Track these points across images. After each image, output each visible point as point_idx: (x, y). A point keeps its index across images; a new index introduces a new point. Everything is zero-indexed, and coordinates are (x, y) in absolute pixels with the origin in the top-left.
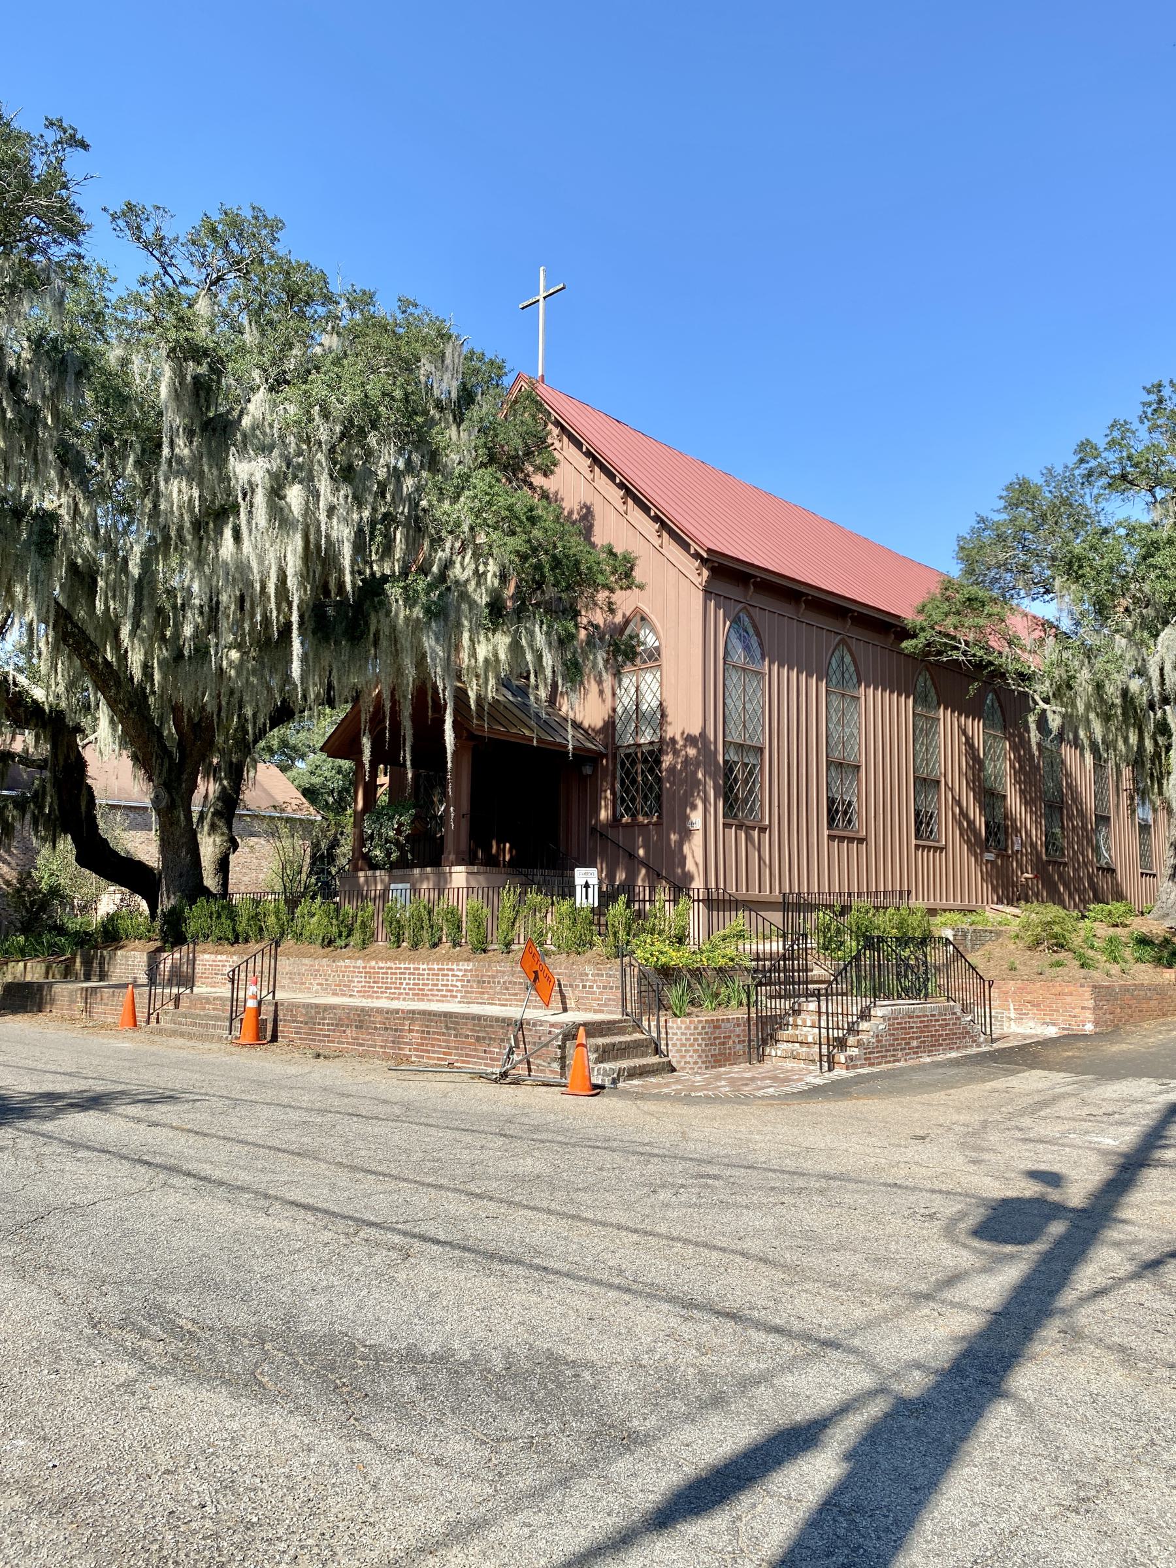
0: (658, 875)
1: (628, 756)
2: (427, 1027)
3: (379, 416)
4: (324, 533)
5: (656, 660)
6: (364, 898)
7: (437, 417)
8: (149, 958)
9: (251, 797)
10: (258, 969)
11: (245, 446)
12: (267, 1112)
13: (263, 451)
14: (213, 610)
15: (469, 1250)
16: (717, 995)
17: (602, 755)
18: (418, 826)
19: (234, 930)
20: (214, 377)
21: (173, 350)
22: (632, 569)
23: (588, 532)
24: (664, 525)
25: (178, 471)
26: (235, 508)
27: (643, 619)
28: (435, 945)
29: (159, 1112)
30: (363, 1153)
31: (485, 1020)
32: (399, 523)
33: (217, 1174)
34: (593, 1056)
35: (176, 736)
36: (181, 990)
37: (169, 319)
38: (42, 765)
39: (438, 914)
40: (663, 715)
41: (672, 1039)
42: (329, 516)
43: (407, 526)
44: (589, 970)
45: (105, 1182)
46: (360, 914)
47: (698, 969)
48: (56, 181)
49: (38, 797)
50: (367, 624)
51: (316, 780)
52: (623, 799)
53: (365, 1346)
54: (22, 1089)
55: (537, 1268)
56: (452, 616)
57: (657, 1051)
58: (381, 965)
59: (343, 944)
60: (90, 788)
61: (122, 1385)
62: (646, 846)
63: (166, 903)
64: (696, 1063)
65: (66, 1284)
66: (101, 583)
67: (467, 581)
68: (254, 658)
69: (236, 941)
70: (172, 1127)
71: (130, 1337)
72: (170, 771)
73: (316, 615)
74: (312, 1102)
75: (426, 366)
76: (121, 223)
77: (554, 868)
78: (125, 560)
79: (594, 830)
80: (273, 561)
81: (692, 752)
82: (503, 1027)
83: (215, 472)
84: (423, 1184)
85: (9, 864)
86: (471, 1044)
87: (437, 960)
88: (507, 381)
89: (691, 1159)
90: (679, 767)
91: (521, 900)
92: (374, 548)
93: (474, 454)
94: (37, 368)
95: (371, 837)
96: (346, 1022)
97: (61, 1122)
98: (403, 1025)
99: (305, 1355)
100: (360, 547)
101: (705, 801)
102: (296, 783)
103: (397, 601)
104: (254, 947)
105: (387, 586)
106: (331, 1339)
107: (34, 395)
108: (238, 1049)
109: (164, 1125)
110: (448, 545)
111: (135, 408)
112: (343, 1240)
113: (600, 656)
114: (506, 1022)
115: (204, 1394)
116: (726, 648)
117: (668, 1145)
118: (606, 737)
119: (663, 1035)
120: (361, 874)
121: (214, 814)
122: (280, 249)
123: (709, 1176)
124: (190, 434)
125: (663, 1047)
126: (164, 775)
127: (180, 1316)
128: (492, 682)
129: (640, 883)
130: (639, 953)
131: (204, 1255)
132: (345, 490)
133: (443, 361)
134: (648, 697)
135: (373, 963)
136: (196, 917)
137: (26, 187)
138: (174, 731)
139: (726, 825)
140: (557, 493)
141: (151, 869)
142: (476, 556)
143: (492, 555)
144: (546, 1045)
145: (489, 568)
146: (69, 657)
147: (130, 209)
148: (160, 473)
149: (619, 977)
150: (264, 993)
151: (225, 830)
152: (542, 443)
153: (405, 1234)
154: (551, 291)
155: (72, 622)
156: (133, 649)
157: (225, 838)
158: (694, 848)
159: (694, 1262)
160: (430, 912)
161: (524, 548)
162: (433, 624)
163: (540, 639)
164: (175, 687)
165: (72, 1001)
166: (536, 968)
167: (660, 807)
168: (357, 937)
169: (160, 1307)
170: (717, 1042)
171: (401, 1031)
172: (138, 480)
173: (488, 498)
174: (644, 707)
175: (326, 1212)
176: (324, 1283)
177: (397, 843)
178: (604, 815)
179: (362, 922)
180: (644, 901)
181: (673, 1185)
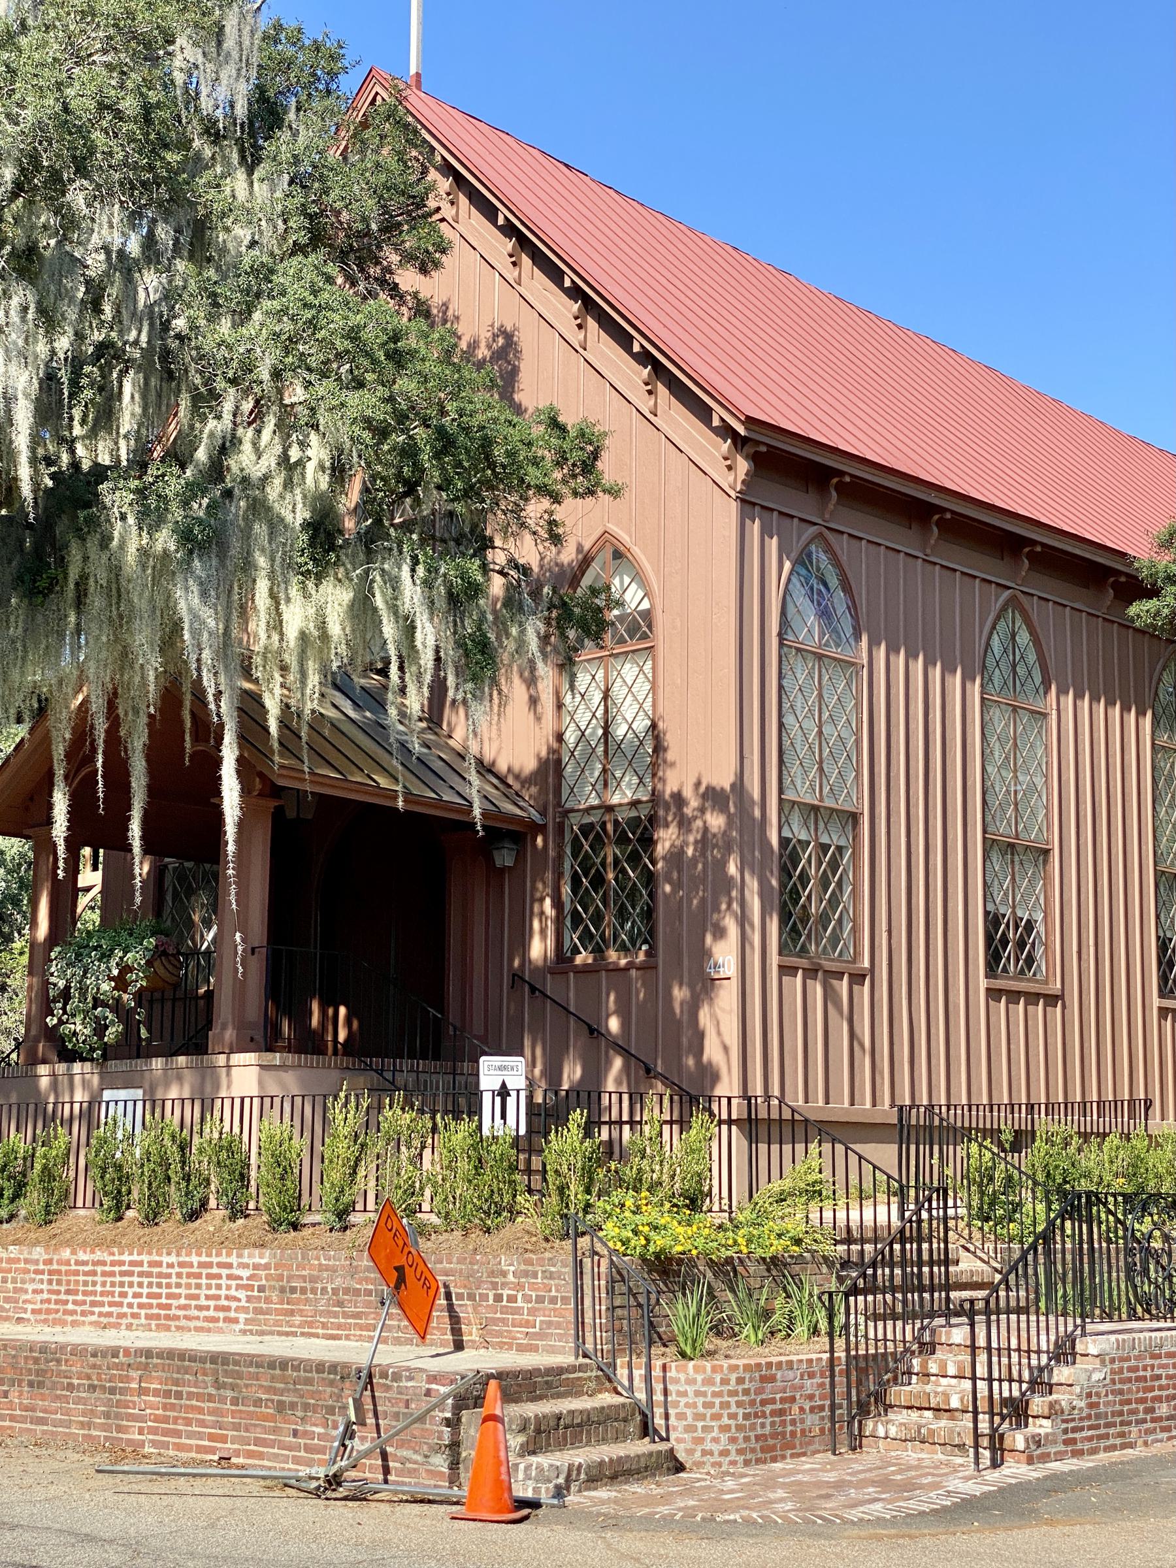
1: (586, 829)
2: (176, 1383)
5: (645, 637)
6: (49, 1120)
16: (767, 1314)
18: (161, 971)
22: (595, 455)
23: (506, 384)
27: (618, 555)
28: (193, 1215)
31: (296, 1368)
32: (128, 364)
40: (659, 748)
41: (676, 1404)
43: (145, 368)
44: (510, 1265)
46: (40, 1151)
47: (729, 1261)
50: (62, 563)
57: (646, 1429)
58: (82, 1256)
62: (624, 1012)
64: (724, 1453)
67: (266, 478)
77: (436, 1057)
79: (517, 978)
81: (716, 821)
82: (332, 1383)
86: (266, 1418)
87: (198, 1247)
88: (348, 84)
90: (690, 852)
92: (77, 413)
93: (281, 226)
95: (66, 995)
101: (743, 921)
103: (123, 517)
105: (103, 487)
110: (228, 407)
113: (533, 628)
114: (337, 1372)
116: (783, 613)
118: (543, 791)
119: (658, 1397)
120: (43, 1070)
125: (659, 1421)
128: (314, 679)
129: (610, 1086)
133: (219, 44)
134: (629, 710)
135: (66, 1253)
140: (445, 305)
142: (285, 428)
143: (315, 427)
144: (421, 1419)
145: (309, 453)
149: (569, 1278)
160: (184, 1147)
161: (381, 414)
163: (412, 594)
167: (652, 932)
168: (34, 1198)
170: (768, 1409)
171: (123, 1391)
173: (308, 314)
174: (620, 731)
177: (117, 1007)
178: (539, 948)
179: (45, 1168)
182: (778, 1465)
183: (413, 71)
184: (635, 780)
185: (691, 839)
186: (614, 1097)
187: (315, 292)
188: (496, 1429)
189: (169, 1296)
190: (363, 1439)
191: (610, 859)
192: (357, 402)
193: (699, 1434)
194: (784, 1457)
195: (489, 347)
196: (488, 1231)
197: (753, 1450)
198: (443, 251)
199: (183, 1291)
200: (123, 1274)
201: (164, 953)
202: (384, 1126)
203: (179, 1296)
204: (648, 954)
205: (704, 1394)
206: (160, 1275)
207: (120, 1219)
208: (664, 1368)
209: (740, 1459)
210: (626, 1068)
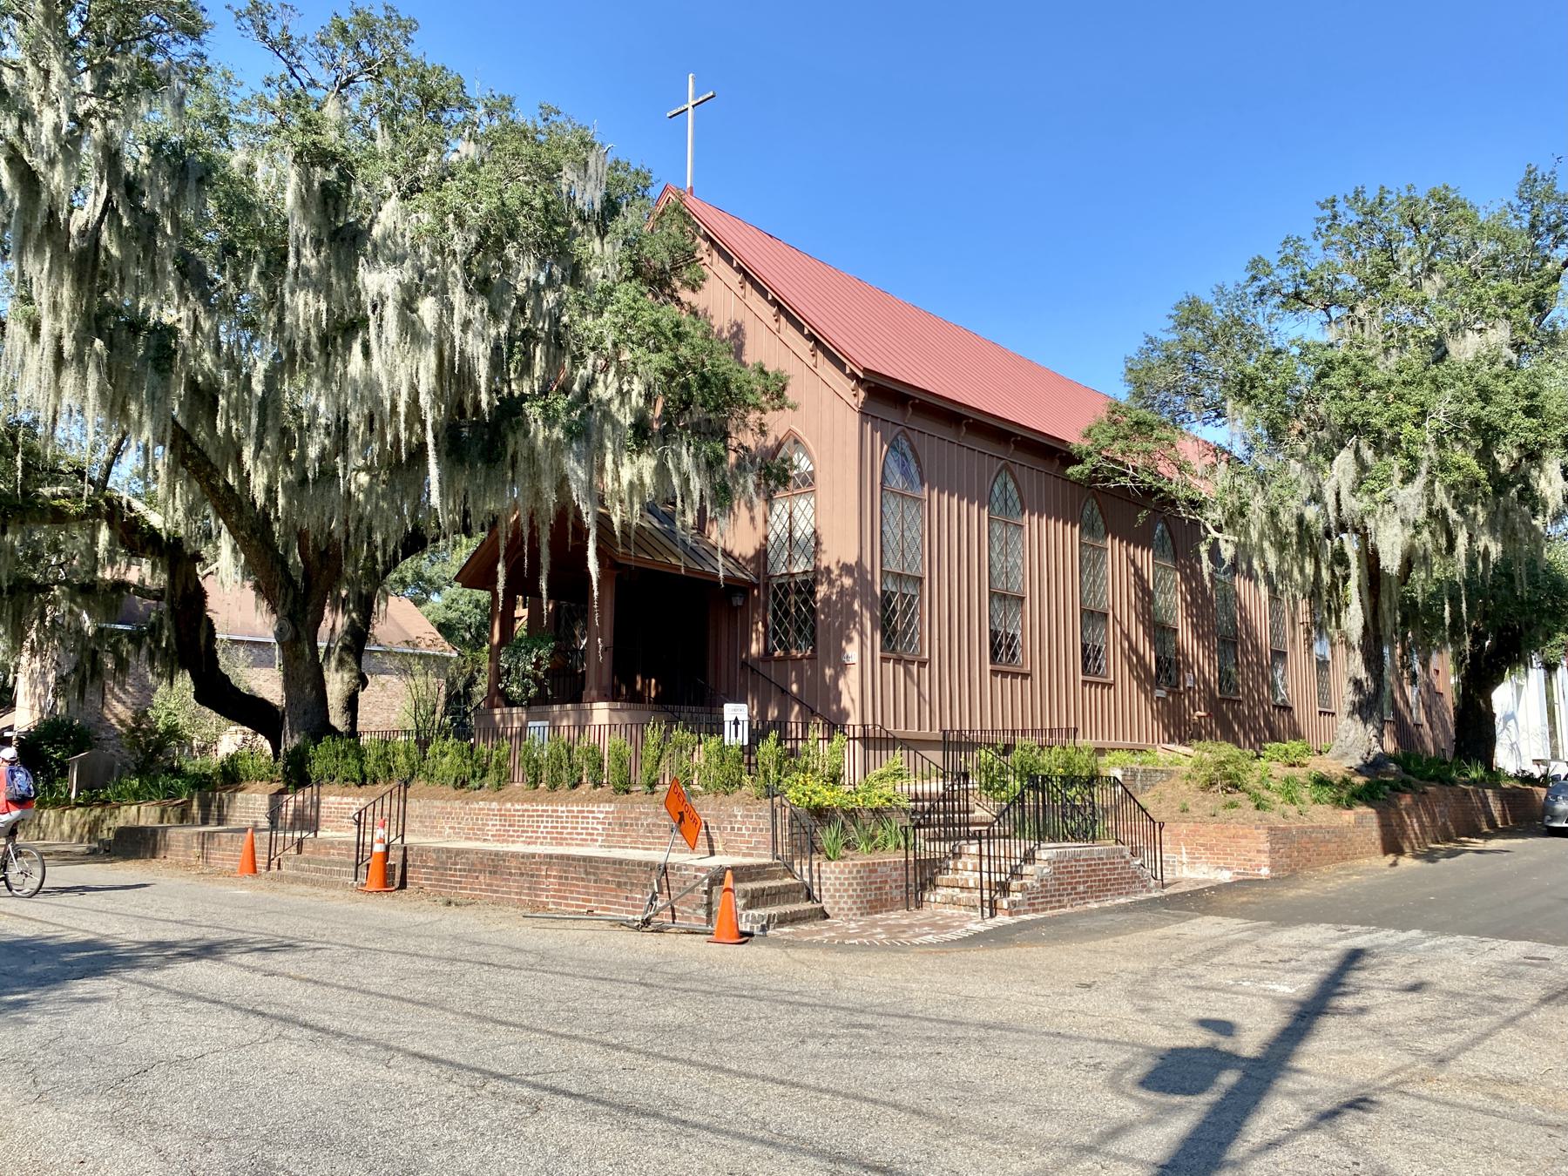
0: (812, 712)
1: (780, 586)
2: (565, 872)
3: (517, 225)
4: (457, 349)
5: (810, 485)
7: (580, 229)
8: (271, 800)
10: (386, 812)
12: (392, 961)
13: (394, 262)
14: (341, 431)
16: (873, 838)
17: (753, 586)
19: (361, 771)
20: (344, 184)
21: (299, 155)
22: (784, 388)
23: (738, 351)
25: (304, 283)
28: (575, 786)
29: (277, 960)
30: (493, 1003)
31: (627, 864)
33: (336, 1025)
34: (741, 902)
37: (296, 122)
38: (158, 595)
39: (578, 752)
40: (818, 543)
42: (464, 331)
43: (547, 343)
44: (739, 812)
45: (215, 1033)
47: (853, 810)
49: (155, 631)
51: (452, 615)
54: (130, 937)
55: (676, 1121)
56: (595, 437)
57: (809, 897)
59: (477, 785)
60: (210, 621)
62: (799, 682)
63: (290, 742)
65: (168, 1140)
66: (222, 402)
67: (610, 400)
68: (384, 482)
69: (364, 782)
72: (295, 601)
75: (568, 175)
77: (702, 705)
78: (248, 377)
79: (744, 664)
80: (403, 378)
81: (848, 582)
82: (645, 872)
83: (344, 284)
84: (556, 1035)
86: (611, 890)
87: (577, 802)
88: (654, 192)
89: (843, 1008)
93: (618, 267)
94: (156, 173)
95: (508, 672)
96: (479, 867)
97: (171, 971)
101: (862, 634)
102: (431, 617)
103: (536, 421)
104: (382, 788)
105: (526, 405)
109: (282, 974)
110: (590, 362)
112: (469, 1093)
113: (751, 479)
114: (649, 866)
116: (883, 472)
118: (758, 565)
119: (816, 880)
120: (497, 711)
121: (342, 649)
122: (414, 51)
124: (318, 243)
125: (816, 893)
126: (289, 606)
128: (637, 507)
129: (793, 719)
132: (481, 303)
135: (509, 805)
136: (322, 758)
138: (299, 559)
139: (883, 659)
140: (706, 310)
142: (620, 373)
143: (636, 373)
148: (286, 285)
149: (770, 819)
150: (393, 837)
152: (690, 257)
153: (535, 1086)
154: (701, 99)
155: (191, 444)
156: (256, 471)
157: (354, 674)
160: (569, 751)
161: (670, 366)
162: (574, 445)
163: (687, 462)
165: (188, 847)
168: (492, 778)
170: (873, 887)
171: (538, 876)
173: (632, 312)
174: (797, 534)
175: (451, 1064)
176: (447, 1138)
177: (536, 679)
178: (755, 648)
182: (878, 916)
186: (794, 725)
187: (635, 301)
189: (562, 828)
196: (727, 794)
201: (559, 651)
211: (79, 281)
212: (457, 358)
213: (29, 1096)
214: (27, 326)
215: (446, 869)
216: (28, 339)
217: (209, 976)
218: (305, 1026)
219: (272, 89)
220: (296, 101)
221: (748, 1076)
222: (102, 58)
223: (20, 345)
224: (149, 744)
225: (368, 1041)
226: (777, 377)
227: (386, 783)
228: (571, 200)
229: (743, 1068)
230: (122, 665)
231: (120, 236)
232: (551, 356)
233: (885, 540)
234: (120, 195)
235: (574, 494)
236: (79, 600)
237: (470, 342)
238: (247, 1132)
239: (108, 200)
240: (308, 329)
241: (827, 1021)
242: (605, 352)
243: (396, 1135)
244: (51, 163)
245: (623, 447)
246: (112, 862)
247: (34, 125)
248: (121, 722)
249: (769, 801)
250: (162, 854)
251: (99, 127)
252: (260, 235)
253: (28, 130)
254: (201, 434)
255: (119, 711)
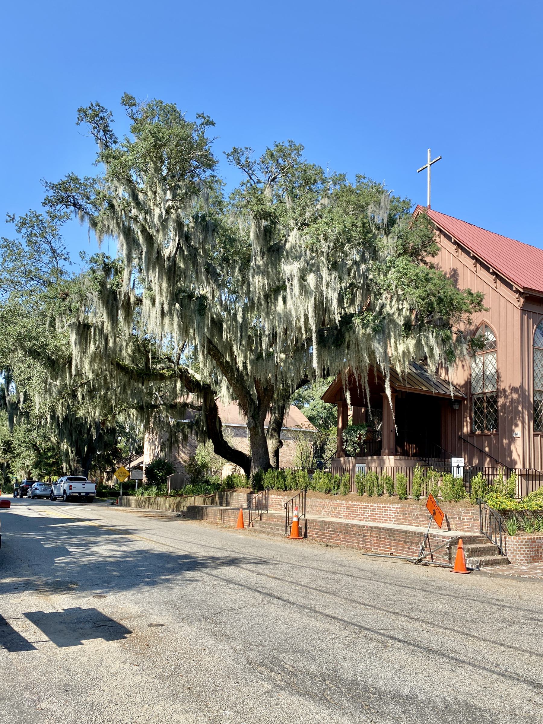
0: (496, 461)
1: (478, 399)
2: (379, 535)
3: (351, 236)
4: (325, 296)
5: (494, 348)
6: (344, 471)
7: (377, 233)
8: (248, 496)
9: (288, 422)
10: (297, 503)
11: (288, 258)
12: (308, 572)
13: (296, 259)
14: (274, 336)
15: (416, 646)
16: (532, 525)
17: (464, 399)
18: (369, 436)
19: (285, 484)
20: (273, 226)
21: (255, 215)
22: (481, 301)
23: (455, 282)
24: (497, 276)
25: (258, 272)
26: (284, 288)
27: (486, 326)
28: (380, 495)
29: (261, 568)
30: (357, 594)
31: (409, 533)
32: (358, 288)
33: (291, 599)
34: (466, 554)
35: (256, 394)
36: (263, 512)
37: (254, 201)
38: (199, 409)
39: (382, 480)
41: (508, 547)
42: (327, 288)
43: (362, 288)
44: (462, 510)
45: (243, 599)
46: (343, 478)
47: (522, 511)
48: (202, 143)
49: (197, 422)
50: (343, 338)
51: (315, 413)
52: (476, 422)
53: (373, 688)
54: (201, 554)
55: (453, 659)
56: (387, 332)
57: (500, 553)
58: (354, 503)
59: (335, 493)
60: (219, 419)
61: (266, 692)
62: (489, 446)
63: (254, 471)
64: (522, 560)
65: (234, 643)
66: (225, 326)
67: (394, 314)
68: (291, 357)
69: (286, 490)
70: (268, 576)
71: (266, 671)
72: (254, 410)
73: (319, 335)
74: (329, 568)
75: (371, 208)
76: (231, 158)
77: (439, 458)
78: (235, 315)
79: (460, 438)
80: (302, 311)
81: (515, 396)
82: (418, 537)
83: (274, 271)
84: (388, 612)
85: (184, 453)
86: (402, 544)
87: (382, 502)
88: (411, 210)
89: (527, 610)
90: (508, 404)
91: (425, 474)
92: (345, 301)
93: (395, 249)
94: (196, 230)
95: (346, 441)
96: (339, 530)
97: (220, 570)
98: (367, 533)
99: (345, 688)
100: (340, 301)
101: (523, 422)
102: (305, 414)
103: (358, 326)
104: (294, 492)
105: (353, 319)
106: (356, 683)
107: (195, 243)
108: (290, 540)
109: (264, 575)
110: (384, 296)
111: (238, 244)
112: (354, 636)
113: (465, 347)
114: (419, 535)
115: (303, 701)
116: (534, 340)
117: (512, 601)
118: (466, 389)
119: (503, 545)
120: (342, 459)
122: (301, 160)
123: (538, 620)
124: (263, 254)
125: (504, 551)
126: (252, 412)
127: (286, 664)
128: (407, 363)
129: (486, 466)
130: (489, 502)
131: (292, 637)
132: (335, 274)
133: (380, 204)
134: (490, 368)
135: (350, 502)
136: (268, 478)
137: (191, 148)
138: (256, 392)
139: (535, 435)
140: (438, 264)
141: (246, 455)
142: (398, 300)
143: (406, 299)
144: (441, 547)
145: (404, 306)
146: (211, 361)
147: (235, 151)
148: (250, 274)
149: (479, 514)
150: (300, 514)
151: (277, 437)
152: (431, 240)
153: (383, 635)
154: (434, 161)
155: (212, 345)
156: (239, 355)
157: (277, 441)
158: (517, 447)
159: (537, 664)
160: (377, 479)
161: (424, 295)
162: (377, 336)
163: (432, 341)
164: (257, 372)
165: (216, 515)
166: (434, 508)
167: (497, 426)
168: (342, 489)
169: (277, 659)
170: (534, 549)
171: (366, 536)
172: (240, 278)
173: (405, 271)
174: (488, 373)
175: (344, 621)
176: (349, 655)
177: (359, 444)
178: (465, 430)
179: (344, 482)
180: (488, 475)
181: (519, 623)
182: (537, 564)
183: (428, 204)
184: (492, 386)
185: (508, 401)
186: (487, 469)
187: (406, 265)
188: (461, 552)
189: (375, 514)
190: (426, 551)
191: (485, 406)
192: (418, 292)
193: (515, 555)
194: (538, 562)
195: (450, 274)
196: (456, 502)
197: (530, 560)
198: (438, 251)
199: (379, 513)
200: (364, 508)
201: (370, 431)
202: (428, 475)
203: (377, 514)
204: (496, 431)
205: (516, 545)
206: (373, 509)
207: (362, 495)
208: (505, 537)
209: (526, 562)
210: (490, 460)
211: (169, 280)
212: (324, 301)
213: (178, 619)
214: (151, 300)
215: (324, 530)
216: (151, 306)
217: (236, 573)
218: (279, 598)
219: (244, 187)
220: (253, 190)
221: (484, 640)
222: (175, 183)
223: (148, 308)
224: (196, 470)
225: (306, 607)
226: (478, 295)
227: (295, 490)
228: (373, 220)
229: (481, 635)
230: (185, 438)
231: (184, 259)
232: (364, 294)
233: (535, 375)
234: (183, 241)
235: (378, 360)
236: (170, 411)
237: (330, 293)
238: (265, 643)
239: (179, 244)
240: (260, 293)
241: (520, 616)
242: (391, 291)
243: (327, 652)
244: (158, 231)
245: (400, 335)
246: (187, 521)
247: (151, 215)
248: (185, 462)
249: (478, 506)
250: (205, 518)
251: (174, 213)
252: (238, 252)
253: (148, 218)
254: (216, 340)
255: (183, 456)
